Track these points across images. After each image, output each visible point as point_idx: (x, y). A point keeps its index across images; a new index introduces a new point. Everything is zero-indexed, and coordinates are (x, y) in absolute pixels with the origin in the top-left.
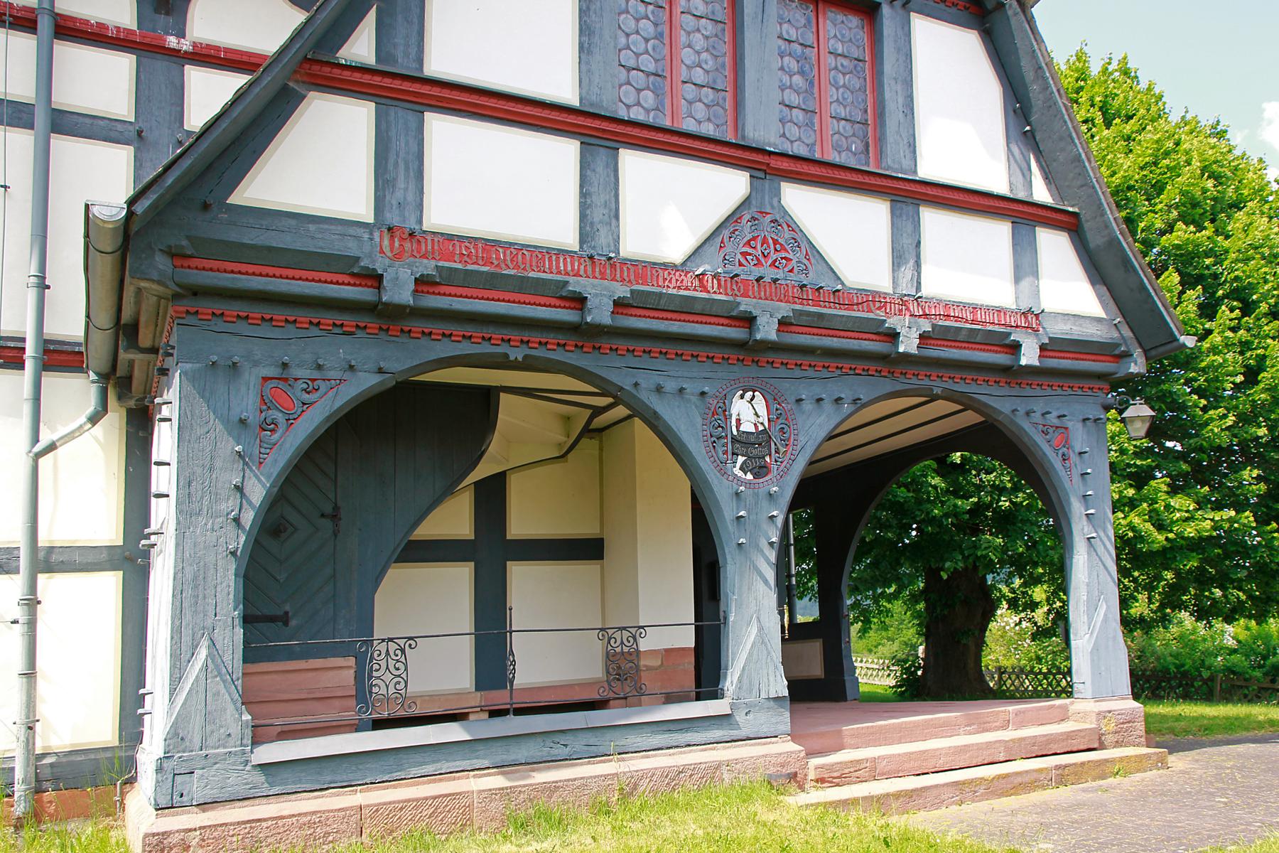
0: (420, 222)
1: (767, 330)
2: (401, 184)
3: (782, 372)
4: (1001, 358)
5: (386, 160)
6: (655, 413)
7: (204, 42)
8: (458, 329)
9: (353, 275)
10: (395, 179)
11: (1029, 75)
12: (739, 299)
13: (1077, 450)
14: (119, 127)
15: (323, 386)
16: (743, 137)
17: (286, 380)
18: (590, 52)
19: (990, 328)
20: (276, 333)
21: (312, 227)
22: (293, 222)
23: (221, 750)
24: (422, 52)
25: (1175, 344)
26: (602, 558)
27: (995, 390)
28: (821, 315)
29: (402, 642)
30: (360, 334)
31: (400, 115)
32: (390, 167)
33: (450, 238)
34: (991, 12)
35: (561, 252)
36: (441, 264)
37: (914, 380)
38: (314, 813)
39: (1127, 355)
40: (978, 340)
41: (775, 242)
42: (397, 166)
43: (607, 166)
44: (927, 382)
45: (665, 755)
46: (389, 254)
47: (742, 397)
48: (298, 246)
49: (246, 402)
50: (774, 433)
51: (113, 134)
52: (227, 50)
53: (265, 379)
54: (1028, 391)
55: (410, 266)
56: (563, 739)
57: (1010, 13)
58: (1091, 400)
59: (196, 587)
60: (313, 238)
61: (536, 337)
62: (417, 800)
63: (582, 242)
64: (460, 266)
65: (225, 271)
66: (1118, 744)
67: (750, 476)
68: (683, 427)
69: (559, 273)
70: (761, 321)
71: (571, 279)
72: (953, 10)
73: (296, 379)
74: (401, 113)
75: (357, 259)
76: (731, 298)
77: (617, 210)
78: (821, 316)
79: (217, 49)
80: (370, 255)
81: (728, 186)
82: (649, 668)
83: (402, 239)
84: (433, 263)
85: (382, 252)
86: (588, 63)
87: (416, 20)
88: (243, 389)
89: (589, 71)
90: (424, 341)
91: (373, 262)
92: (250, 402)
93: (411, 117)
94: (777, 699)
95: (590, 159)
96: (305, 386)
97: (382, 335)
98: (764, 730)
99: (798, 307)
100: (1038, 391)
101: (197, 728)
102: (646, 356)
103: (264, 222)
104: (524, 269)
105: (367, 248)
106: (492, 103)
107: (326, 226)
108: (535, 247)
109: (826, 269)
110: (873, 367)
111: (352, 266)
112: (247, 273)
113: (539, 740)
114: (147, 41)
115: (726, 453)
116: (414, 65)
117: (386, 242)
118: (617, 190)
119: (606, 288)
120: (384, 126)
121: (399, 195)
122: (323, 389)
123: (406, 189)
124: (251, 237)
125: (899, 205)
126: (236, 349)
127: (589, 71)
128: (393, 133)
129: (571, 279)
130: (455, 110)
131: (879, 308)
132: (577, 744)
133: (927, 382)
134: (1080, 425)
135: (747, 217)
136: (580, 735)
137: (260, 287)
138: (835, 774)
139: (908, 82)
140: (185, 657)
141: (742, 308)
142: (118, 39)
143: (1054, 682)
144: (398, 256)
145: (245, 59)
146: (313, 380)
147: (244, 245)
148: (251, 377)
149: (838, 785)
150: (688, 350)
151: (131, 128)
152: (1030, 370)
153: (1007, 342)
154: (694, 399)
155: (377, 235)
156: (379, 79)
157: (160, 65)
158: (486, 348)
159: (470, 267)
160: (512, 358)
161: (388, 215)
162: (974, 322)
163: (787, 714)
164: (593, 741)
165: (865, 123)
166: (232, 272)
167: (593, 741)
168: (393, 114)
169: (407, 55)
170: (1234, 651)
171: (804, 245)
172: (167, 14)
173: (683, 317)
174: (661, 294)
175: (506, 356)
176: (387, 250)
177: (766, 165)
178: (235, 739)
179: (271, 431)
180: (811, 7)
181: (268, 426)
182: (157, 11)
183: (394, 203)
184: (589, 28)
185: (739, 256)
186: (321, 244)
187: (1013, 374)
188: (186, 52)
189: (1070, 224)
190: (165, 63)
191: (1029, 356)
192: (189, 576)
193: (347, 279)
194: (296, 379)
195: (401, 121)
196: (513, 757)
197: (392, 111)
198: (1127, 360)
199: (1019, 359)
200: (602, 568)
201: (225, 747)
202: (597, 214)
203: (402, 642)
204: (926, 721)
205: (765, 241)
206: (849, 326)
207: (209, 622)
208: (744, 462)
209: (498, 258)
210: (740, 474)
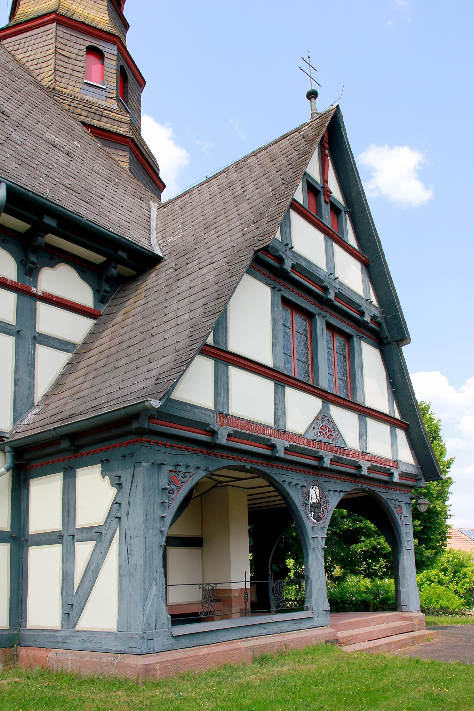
0: (228, 411)
1: (327, 463)
2: (222, 395)
3: (324, 479)
4: (314, 463)
5: (218, 384)
6: (288, 493)
7: (48, 292)
8: (235, 455)
9: (206, 431)
10: (221, 393)
11: (397, 370)
12: (319, 450)
13: (404, 515)
14: (10, 327)
15: (188, 475)
16: (318, 385)
17: (176, 472)
18: (275, 347)
19: (386, 467)
20: (173, 452)
21: (196, 410)
22: (190, 408)
23: (162, 630)
24: (227, 341)
25: (438, 477)
26: (202, 546)
27: (384, 490)
28: (341, 458)
29: (212, 585)
30: (200, 454)
31: (221, 366)
32: (219, 387)
33: (237, 418)
34: (384, 344)
35: (269, 427)
36: (235, 429)
37: (360, 485)
38: (195, 656)
39: (420, 479)
40: (377, 470)
41: (328, 428)
42: (221, 387)
43: (281, 393)
44: (363, 486)
45: (295, 633)
46: (219, 424)
47: (312, 488)
48: (191, 418)
49: (164, 481)
50: (322, 503)
51: (7, 330)
52: (57, 297)
53: (170, 471)
54: (391, 491)
55: (225, 429)
56: (265, 626)
57: (393, 347)
58: (406, 495)
59: (150, 560)
60: (196, 415)
61: (256, 460)
62: (226, 651)
63: (275, 423)
64: (240, 430)
65: (165, 426)
66: (419, 629)
67: (315, 521)
68: (296, 500)
69: (269, 435)
70: (326, 459)
71: (272, 438)
72: (372, 341)
73: (179, 472)
74: (221, 364)
75: (209, 424)
76: (316, 450)
77: (285, 411)
78: (341, 458)
79: (53, 296)
80: (213, 424)
81: (314, 404)
82: (235, 597)
83: (223, 418)
84: (232, 428)
85: (217, 423)
86: (275, 351)
87: (225, 328)
88: (163, 475)
89: (275, 354)
90: (220, 459)
91: (214, 426)
92: (165, 481)
93: (225, 367)
94: (327, 611)
95: (276, 389)
96: (182, 475)
97: (207, 455)
98: (323, 624)
99: (335, 455)
100: (393, 491)
101: (154, 621)
102: (178, 449)
103: (181, 407)
104: (251, 431)
105: (212, 421)
106: (251, 365)
107: (200, 410)
108: (262, 424)
109: (342, 440)
110: (350, 478)
111: (206, 427)
112: (171, 427)
113: (258, 626)
114: (23, 288)
115: (309, 511)
116: (225, 346)
117: (218, 419)
118: (285, 403)
119: (282, 443)
120: (216, 371)
121: (222, 398)
122: (188, 477)
123: (224, 397)
124: (179, 413)
125: (361, 416)
126: (159, 458)
127: (275, 354)
128: (219, 374)
129: (272, 438)
130: (238, 366)
131: (357, 457)
132: (269, 629)
133: (363, 486)
134: (404, 505)
135: (320, 417)
136: (270, 624)
137: (176, 433)
138: (347, 641)
139: (362, 368)
140: (148, 590)
141: (320, 454)
142: (11, 286)
143: (301, 605)
144: (222, 425)
145: (64, 302)
146: (185, 473)
147: (177, 417)
148: (166, 469)
149: (347, 645)
150: (298, 468)
151: (14, 328)
152: (396, 484)
153: (389, 472)
154: (300, 488)
155: (215, 415)
156: (218, 351)
157: (27, 300)
158: (239, 463)
159: (243, 431)
160: (247, 468)
161: (219, 407)
162: (382, 464)
163: (329, 617)
164: (274, 627)
165: (346, 382)
166: (167, 426)
167: (274, 627)
168: (219, 365)
169: (223, 341)
170: (365, 592)
171: (336, 430)
172: (30, 276)
173: (301, 455)
174: (298, 446)
175: (244, 466)
176: (218, 422)
177: (327, 397)
178: (166, 625)
179: (172, 493)
180: (331, 333)
181: (171, 491)
182: (26, 274)
183: (221, 403)
184: (275, 336)
185: (319, 433)
186: (198, 418)
187: (388, 484)
188: (39, 295)
189: (406, 429)
190: (29, 299)
191: (396, 479)
192: (148, 555)
193: (203, 432)
194: (179, 472)
195: (222, 369)
196: (250, 634)
197: (219, 364)
198: (420, 481)
199: (392, 479)
200: (202, 551)
201: (163, 629)
202: (280, 412)
203: (212, 585)
204: (362, 620)
205: (325, 427)
206: (347, 463)
207: (155, 576)
208: (314, 515)
209: (251, 428)
210: (313, 519)
